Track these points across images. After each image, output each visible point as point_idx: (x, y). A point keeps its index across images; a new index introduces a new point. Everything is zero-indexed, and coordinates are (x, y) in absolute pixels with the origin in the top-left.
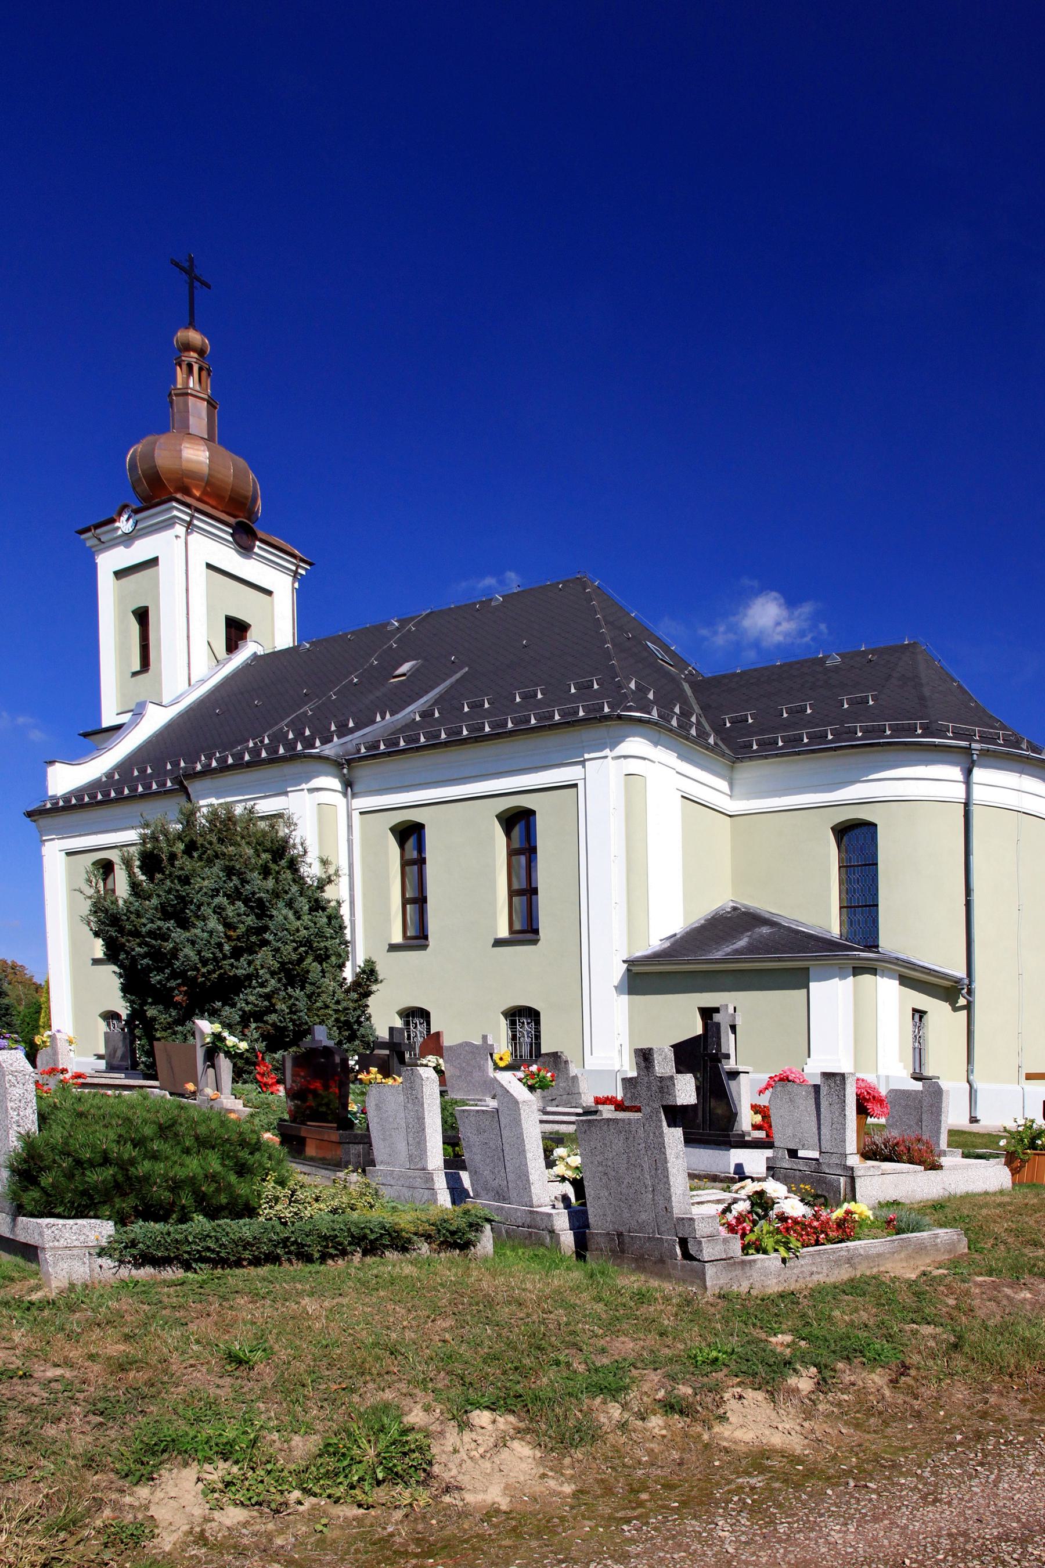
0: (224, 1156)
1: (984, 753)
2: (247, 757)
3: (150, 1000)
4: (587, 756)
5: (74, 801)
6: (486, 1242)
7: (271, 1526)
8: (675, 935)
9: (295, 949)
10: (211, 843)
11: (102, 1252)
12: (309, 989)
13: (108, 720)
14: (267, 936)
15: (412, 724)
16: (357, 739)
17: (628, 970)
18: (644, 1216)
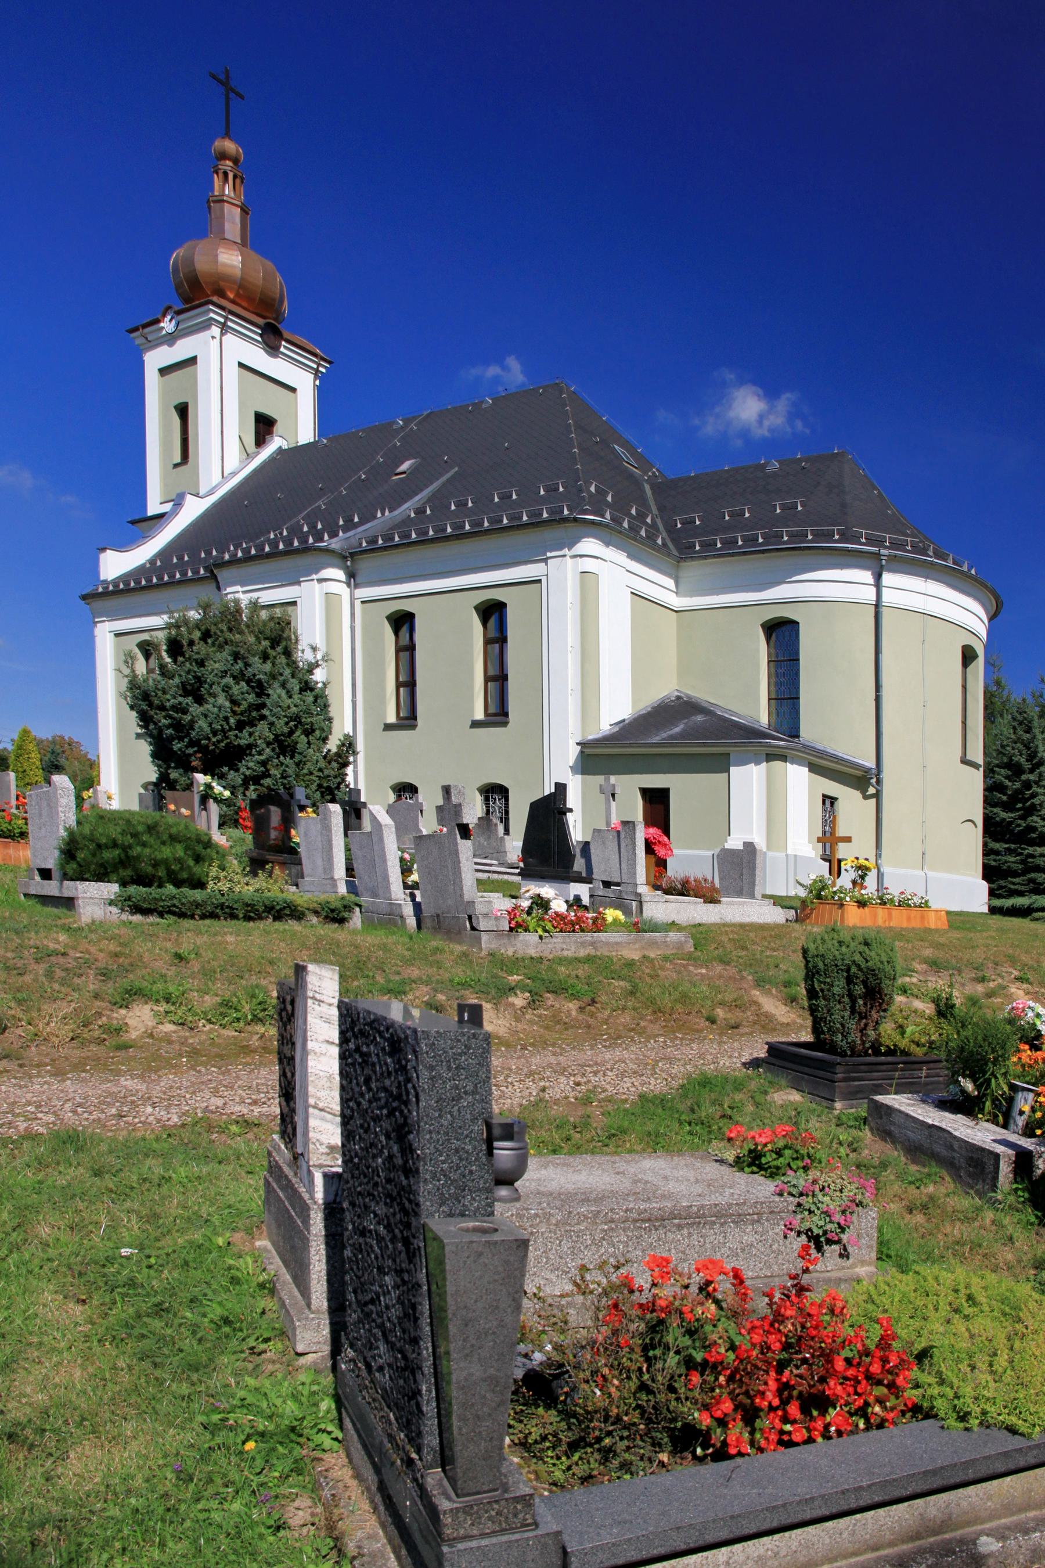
0: (186, 849)
1: (892, 558)
2: (267, 549)
3: (173, 765)
4: (549, 554)
5: (122, 586)
6: (356, 919)
7: (187, 1034)
8: (624, 720)
9: (287, 723)
10: (222, 631)
11: (111, 903)
12: (297, 757)
13: (153, 508)
14: (265, 712)
15: (407, 521)
16: (359, 535)
17: (582, 752)
18: (449, 902)
